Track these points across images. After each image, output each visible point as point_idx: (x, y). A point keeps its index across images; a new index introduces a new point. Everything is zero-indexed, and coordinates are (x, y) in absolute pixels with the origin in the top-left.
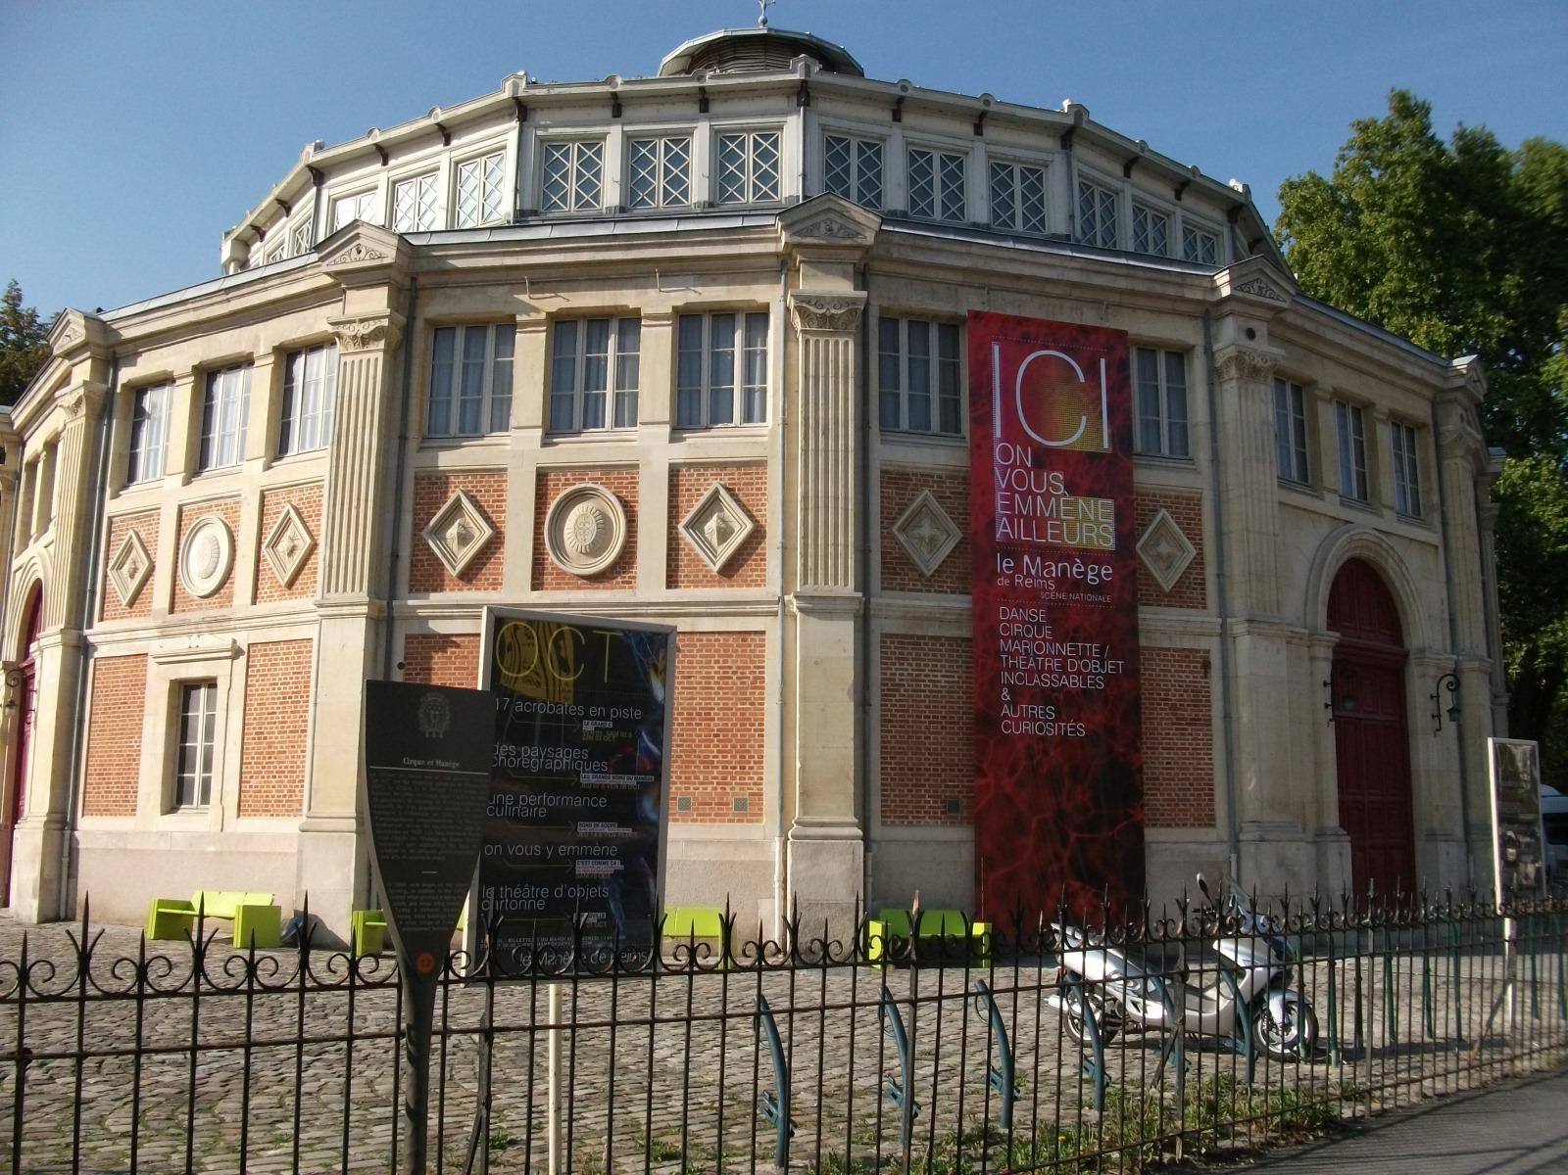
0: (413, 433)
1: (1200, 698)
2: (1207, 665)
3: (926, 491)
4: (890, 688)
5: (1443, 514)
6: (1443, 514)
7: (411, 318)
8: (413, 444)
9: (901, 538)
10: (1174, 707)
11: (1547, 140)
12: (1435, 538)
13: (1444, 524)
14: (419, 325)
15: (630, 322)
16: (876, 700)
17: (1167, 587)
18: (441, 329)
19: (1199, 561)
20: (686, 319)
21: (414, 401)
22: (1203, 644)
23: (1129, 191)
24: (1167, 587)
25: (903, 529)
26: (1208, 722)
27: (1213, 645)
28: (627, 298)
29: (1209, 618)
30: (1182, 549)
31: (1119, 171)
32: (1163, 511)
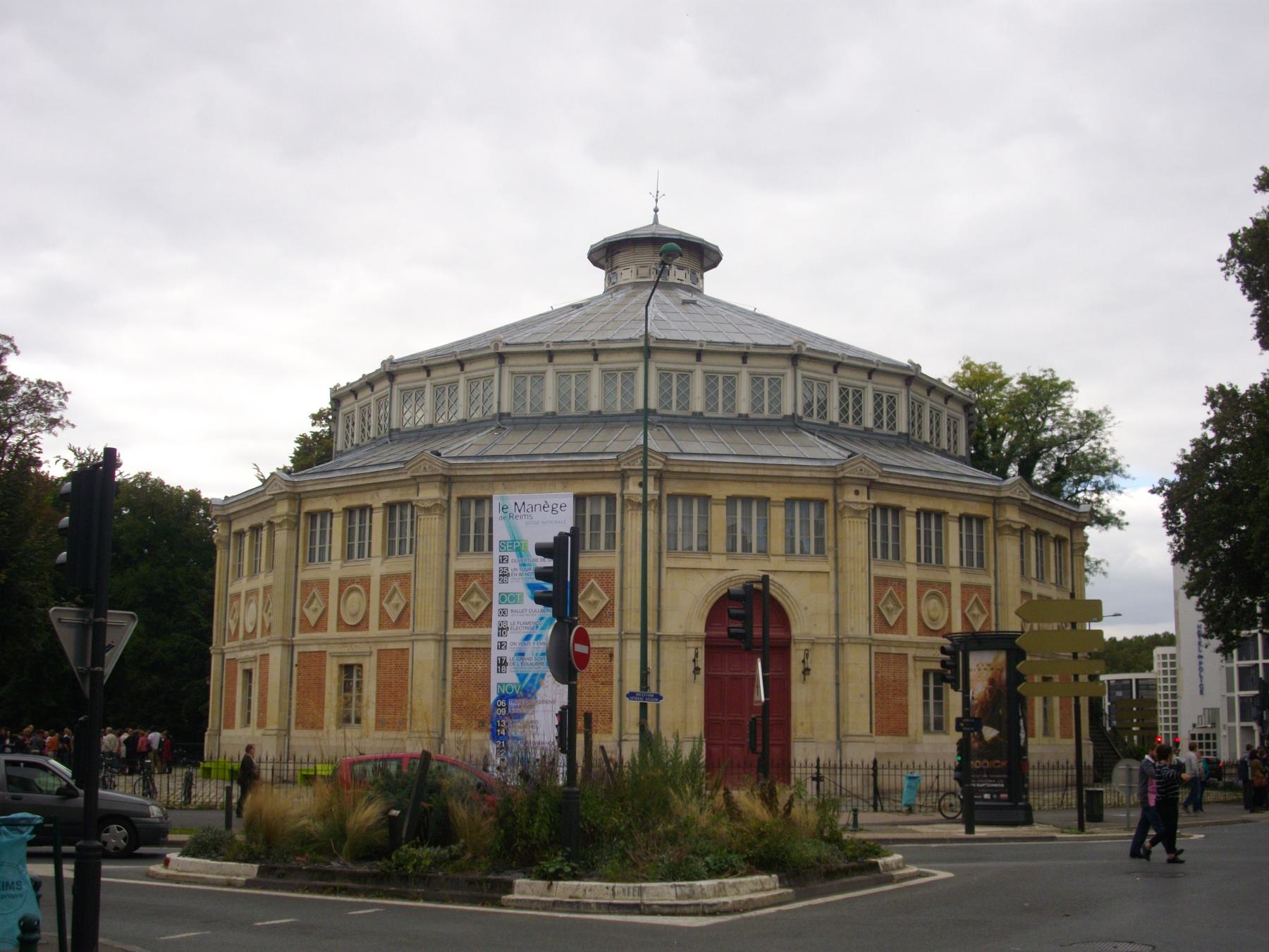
0: (300, 563)
1: (609, 670)
2: (611, 655)
3: (475, 582)
4: (456, 671)
5: (836, 552)
6: (836, 552)
7: (450, 497)
8: (300, 569)
9: (463, 604)
10: (593, 677)
11: (343, 384)
12: (827, 566)
13: (836, 558)
14: (454, 500)
15: (706, 500)
16: (449, 677)
17: (892, 624)
18: (673, 497)
19: (610, 604)
20: (390, 507)
21: (301, 550)
22: (610, 644)
23: (928, 403)
24: (592, 618)
25: (464, 600)
26: (611, 683)
27: (616, 645)
28: (366, 499)
29: (615, 631)
30: (602, 598)
31: (925, 393)
32: (592, 580)
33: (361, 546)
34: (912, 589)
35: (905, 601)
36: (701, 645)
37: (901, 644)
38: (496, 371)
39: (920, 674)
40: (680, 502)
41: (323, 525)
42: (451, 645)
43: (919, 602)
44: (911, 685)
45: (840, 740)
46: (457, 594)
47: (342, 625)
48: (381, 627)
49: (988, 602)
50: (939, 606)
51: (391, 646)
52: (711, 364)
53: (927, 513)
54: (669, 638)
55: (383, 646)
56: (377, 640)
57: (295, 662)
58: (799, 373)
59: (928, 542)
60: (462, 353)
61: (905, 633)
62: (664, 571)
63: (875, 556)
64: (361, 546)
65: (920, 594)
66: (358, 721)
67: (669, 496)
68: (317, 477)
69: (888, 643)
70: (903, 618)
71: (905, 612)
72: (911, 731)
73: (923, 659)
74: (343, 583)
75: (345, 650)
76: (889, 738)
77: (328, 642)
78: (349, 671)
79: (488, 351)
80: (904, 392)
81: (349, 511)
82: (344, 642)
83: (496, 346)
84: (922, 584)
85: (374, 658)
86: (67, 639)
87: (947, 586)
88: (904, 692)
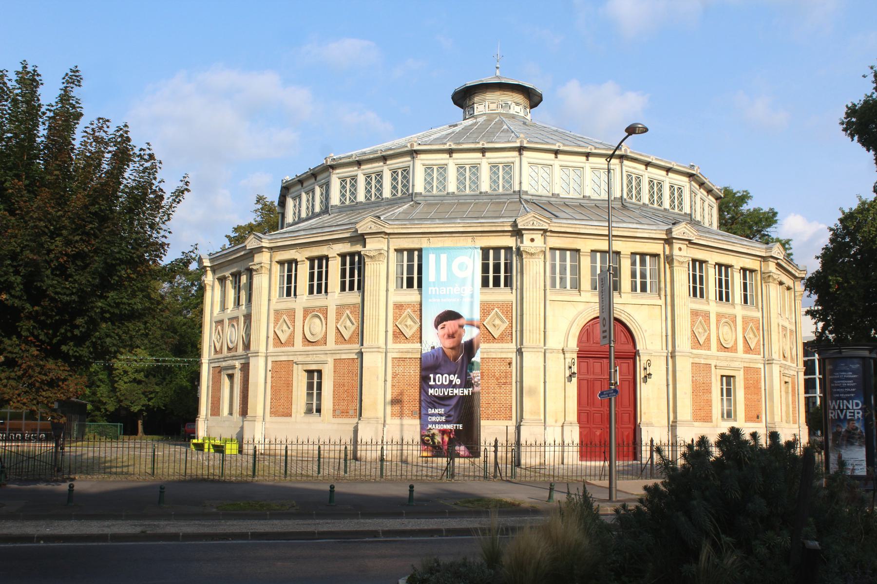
3: (409, 310)
10: (497, 379)
14: (392, 251)
17: (347, 338)
22: (509, 355)
25: (400, 323)
33: (319, 286)
34: (299, 315)
35: (709, 326)
36: (575, 356)
37: (707, 357)
38: (517, 160)
39: (719, 378)
40: (598, 254)
41: (320, 267)
42: (390, 356)
43: (718, 328)
44: (713, 385)
45: (673, 427)
46: (395, 319)
47: (307, 341)
48: (336, 343)
49: (758, 329)
50: (729, 331)
51: (344, 356)
52: (367, 168)
53: (720, 265)
54: (553, 351)
55: (338, 357)
56: (333, 352)
57: (269, 368)
58: (524, 159)
59: (320, 274)
60: (386, 150)
61: (709, 349)
62: (548, 302)
63: (553, 285)
64: (319, 286)
65: (718, 321)
66: (319, 410)
67: (551, 249)
68: (287, 235)
69: (698, 356)
70: (708, 339)
71: (709, 335)
72: (714, 418)
73: (721, 368)
74: (307, 311)
75: (308, 359)
76: (294, 406)
77: (295, 353)
78: (314, 376)
79: (406, 149)
80: (688, 185)
81: (311, 260)
82: (307, 354)
83: (412, 145)
84: (719, 316)
85: (742, 372)
86: (853, 366)
87: (734, 319)
88: (709, 391)
